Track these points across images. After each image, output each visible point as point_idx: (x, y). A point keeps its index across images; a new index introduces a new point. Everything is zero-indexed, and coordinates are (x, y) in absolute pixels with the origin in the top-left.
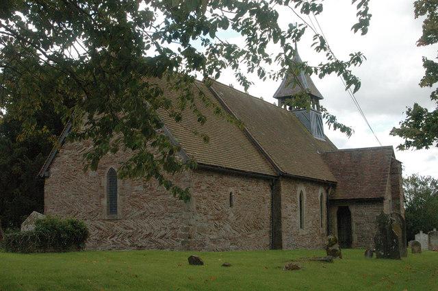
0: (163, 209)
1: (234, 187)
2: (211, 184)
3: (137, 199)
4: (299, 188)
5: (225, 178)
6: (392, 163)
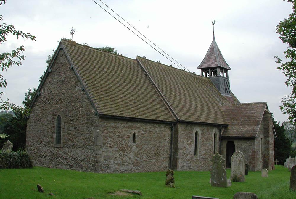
1: (139, 130)
5: (130, 124)
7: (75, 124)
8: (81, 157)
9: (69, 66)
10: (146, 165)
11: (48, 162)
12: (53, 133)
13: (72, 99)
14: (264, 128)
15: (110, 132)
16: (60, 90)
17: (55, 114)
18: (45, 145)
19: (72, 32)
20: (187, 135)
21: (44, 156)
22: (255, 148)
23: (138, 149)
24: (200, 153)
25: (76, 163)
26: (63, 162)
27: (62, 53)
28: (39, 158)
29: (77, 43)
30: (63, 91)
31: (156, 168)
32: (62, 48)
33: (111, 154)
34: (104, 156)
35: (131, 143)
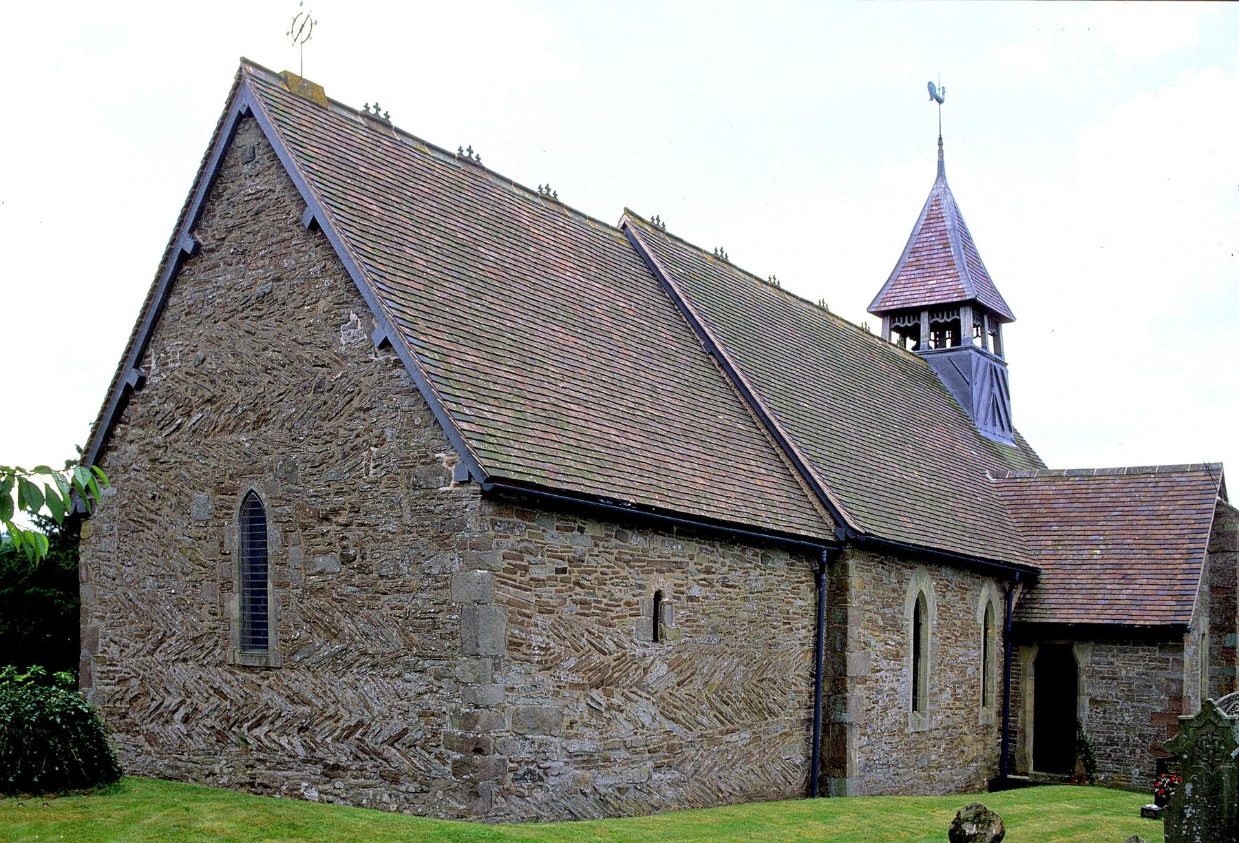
0: (397, 641)
2: (578, 561)
3: (321, 601)
4: (912, 583)
5: (636, 541)
6: (1217, 515)
7: (343, 539)
8: (385, 717)
9: (295, 212)
10: (709, 762)
11: (204, 746)
12: (226, 586)
13: (323, 398)
14: (1213, 588)
15: (539, 582)
16: (251, 353)
17: (228, 483)
18: (182, 656)
19: (302, 29)
20: (882, 611)
21: (178, 716)
22: (1181, 682)
23: (675, 680)
24: (930, 704)
25: (362, 755)
26: (284, 749)
27: (247, 139)
28: (155, 727)
29: (328, 94)
30: (269, 353)
31: (753, 777)
32: (249, 113)
33: (551, 705)
34: (516, 714)
35: (640, 646)
